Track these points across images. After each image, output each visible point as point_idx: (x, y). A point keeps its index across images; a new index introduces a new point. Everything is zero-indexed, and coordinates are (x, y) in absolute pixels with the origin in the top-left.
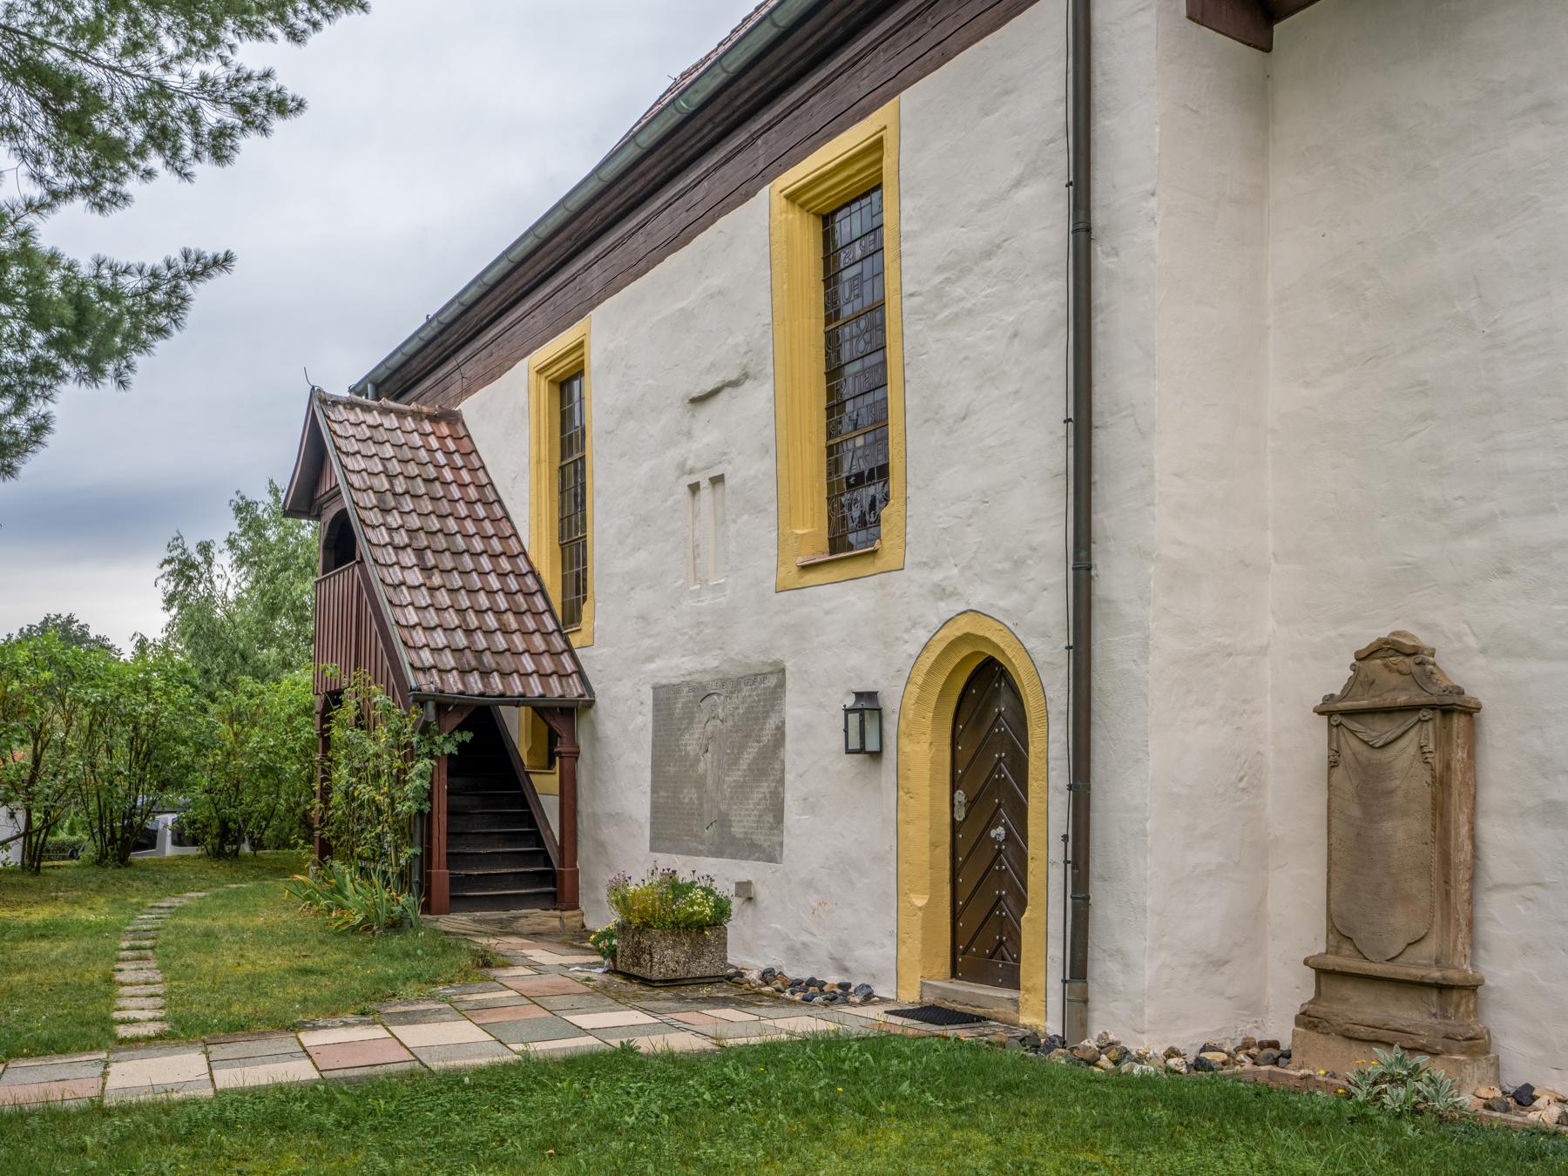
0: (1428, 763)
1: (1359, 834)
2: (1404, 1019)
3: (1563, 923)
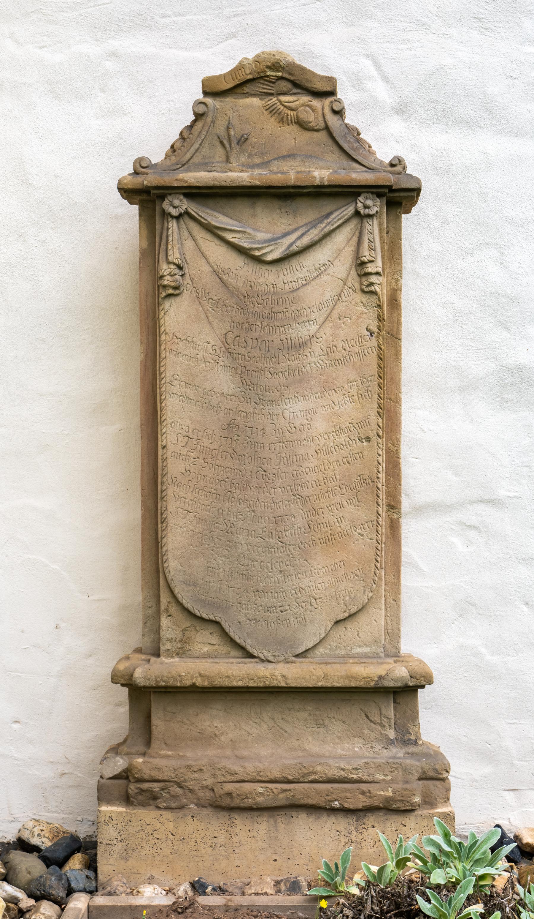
0: (374, 293)
1: (231, 425)
2: (340, 757)
3: (527, 561)
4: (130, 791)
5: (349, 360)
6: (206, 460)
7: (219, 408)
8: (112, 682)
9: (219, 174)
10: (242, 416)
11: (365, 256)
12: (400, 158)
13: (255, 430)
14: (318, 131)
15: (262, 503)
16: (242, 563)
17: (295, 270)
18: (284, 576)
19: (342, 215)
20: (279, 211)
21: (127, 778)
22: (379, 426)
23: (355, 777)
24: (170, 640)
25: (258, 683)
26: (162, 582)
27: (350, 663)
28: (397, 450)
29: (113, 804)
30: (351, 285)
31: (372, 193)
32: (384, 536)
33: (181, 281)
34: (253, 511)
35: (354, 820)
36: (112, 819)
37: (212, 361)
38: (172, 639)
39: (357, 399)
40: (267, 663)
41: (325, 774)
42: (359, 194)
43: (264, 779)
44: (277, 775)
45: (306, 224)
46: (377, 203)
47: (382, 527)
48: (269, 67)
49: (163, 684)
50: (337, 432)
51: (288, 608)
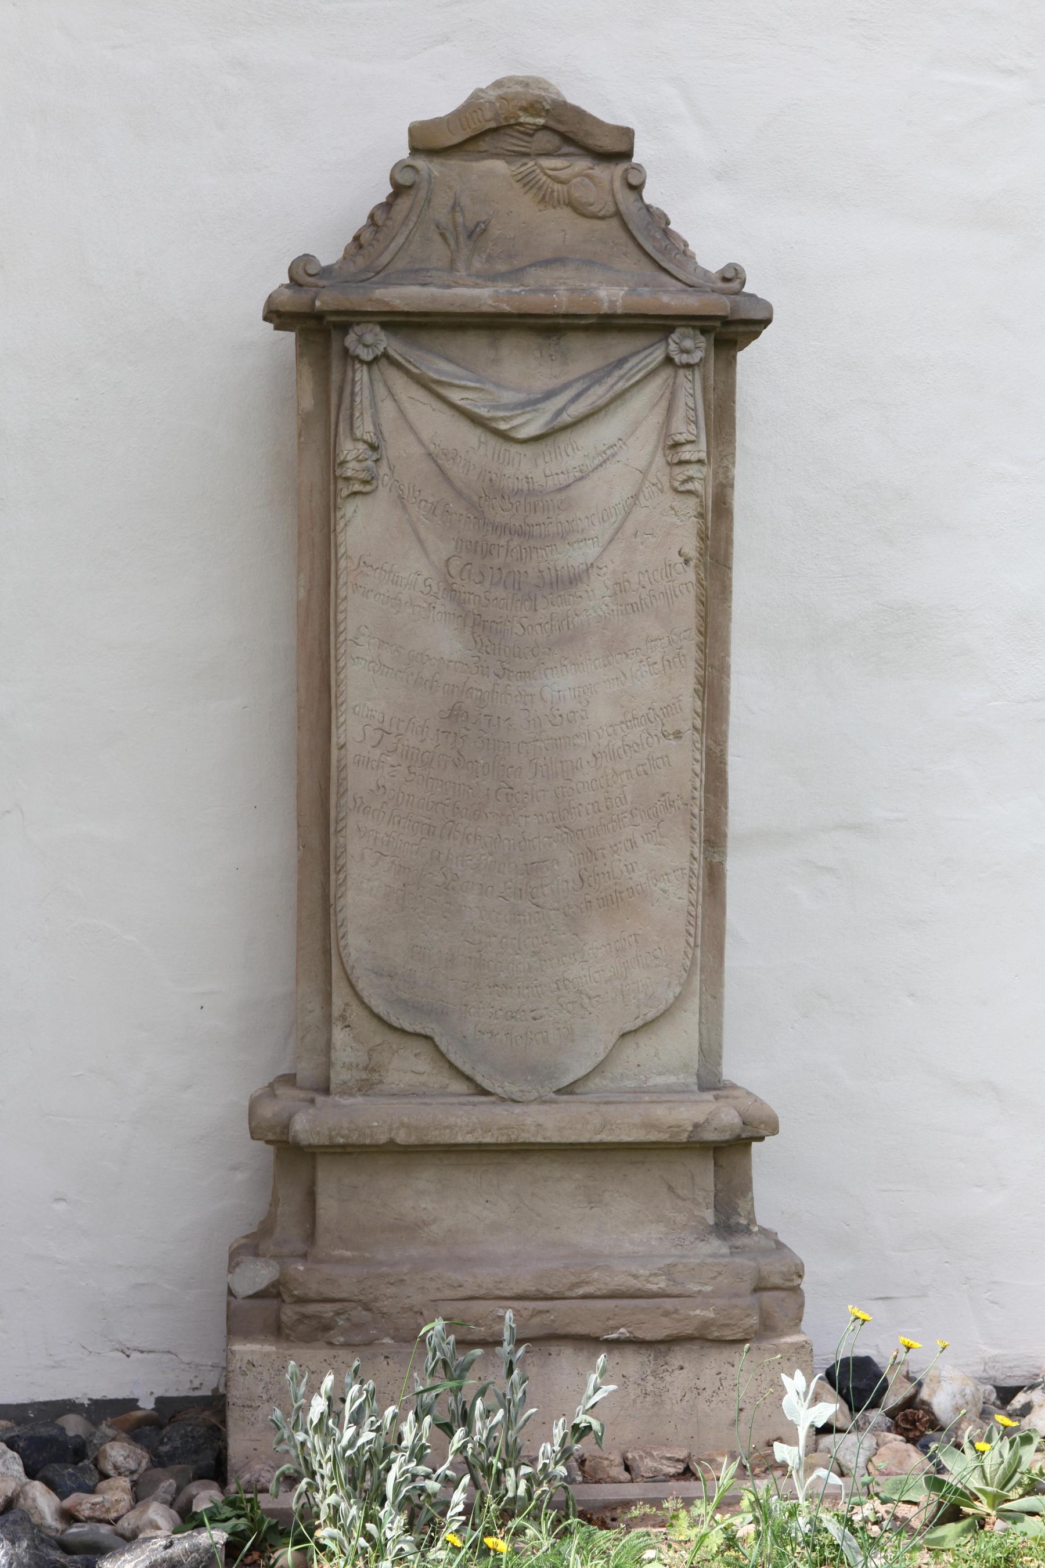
1: (454, 714)
4: (284, 1318)
5: (650, 605)
6: (412, 769)
7: (435, 683)
8: (253, 1138)
9: (441, 290)
10: (474, 696)
11: (680, 434)
12: (738, 268)
13: (495, 721)
14: (603, 218)
15: (506, 842)
16: (470, 940)
17: (564, 454)
18: (541, 960)
19: (644, 363)
20: (537, 354)
21: (278, 1295)
22: (697, 713)
23: (654, 1287)
24: (349, 1067)
25: (498, 1138)
26: (336, 970)
27: (646, 1102)
28: (722, 751)
29: (254, 1341)
30: (655, 481)
31: (694, 327)
32: (700, 893)
33: (375, 469)
34: (491, 854)
35: (651, 1358)
36: (254, 1366)
37: (425, 605)
38: (351, 1065)
39: (662, 668)
40: (511, 1103)
41: (606, 1284)
42: (671, 330)
43: (506, 1294)
44: (531, 1288)
45: (583, 377)
46: (701, 345)
47: (698, 878)
48: (524, 109)
49: (341, 1141)
50: (629, 724)
51: (545, 1012)
